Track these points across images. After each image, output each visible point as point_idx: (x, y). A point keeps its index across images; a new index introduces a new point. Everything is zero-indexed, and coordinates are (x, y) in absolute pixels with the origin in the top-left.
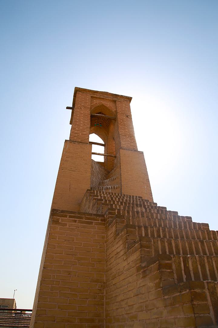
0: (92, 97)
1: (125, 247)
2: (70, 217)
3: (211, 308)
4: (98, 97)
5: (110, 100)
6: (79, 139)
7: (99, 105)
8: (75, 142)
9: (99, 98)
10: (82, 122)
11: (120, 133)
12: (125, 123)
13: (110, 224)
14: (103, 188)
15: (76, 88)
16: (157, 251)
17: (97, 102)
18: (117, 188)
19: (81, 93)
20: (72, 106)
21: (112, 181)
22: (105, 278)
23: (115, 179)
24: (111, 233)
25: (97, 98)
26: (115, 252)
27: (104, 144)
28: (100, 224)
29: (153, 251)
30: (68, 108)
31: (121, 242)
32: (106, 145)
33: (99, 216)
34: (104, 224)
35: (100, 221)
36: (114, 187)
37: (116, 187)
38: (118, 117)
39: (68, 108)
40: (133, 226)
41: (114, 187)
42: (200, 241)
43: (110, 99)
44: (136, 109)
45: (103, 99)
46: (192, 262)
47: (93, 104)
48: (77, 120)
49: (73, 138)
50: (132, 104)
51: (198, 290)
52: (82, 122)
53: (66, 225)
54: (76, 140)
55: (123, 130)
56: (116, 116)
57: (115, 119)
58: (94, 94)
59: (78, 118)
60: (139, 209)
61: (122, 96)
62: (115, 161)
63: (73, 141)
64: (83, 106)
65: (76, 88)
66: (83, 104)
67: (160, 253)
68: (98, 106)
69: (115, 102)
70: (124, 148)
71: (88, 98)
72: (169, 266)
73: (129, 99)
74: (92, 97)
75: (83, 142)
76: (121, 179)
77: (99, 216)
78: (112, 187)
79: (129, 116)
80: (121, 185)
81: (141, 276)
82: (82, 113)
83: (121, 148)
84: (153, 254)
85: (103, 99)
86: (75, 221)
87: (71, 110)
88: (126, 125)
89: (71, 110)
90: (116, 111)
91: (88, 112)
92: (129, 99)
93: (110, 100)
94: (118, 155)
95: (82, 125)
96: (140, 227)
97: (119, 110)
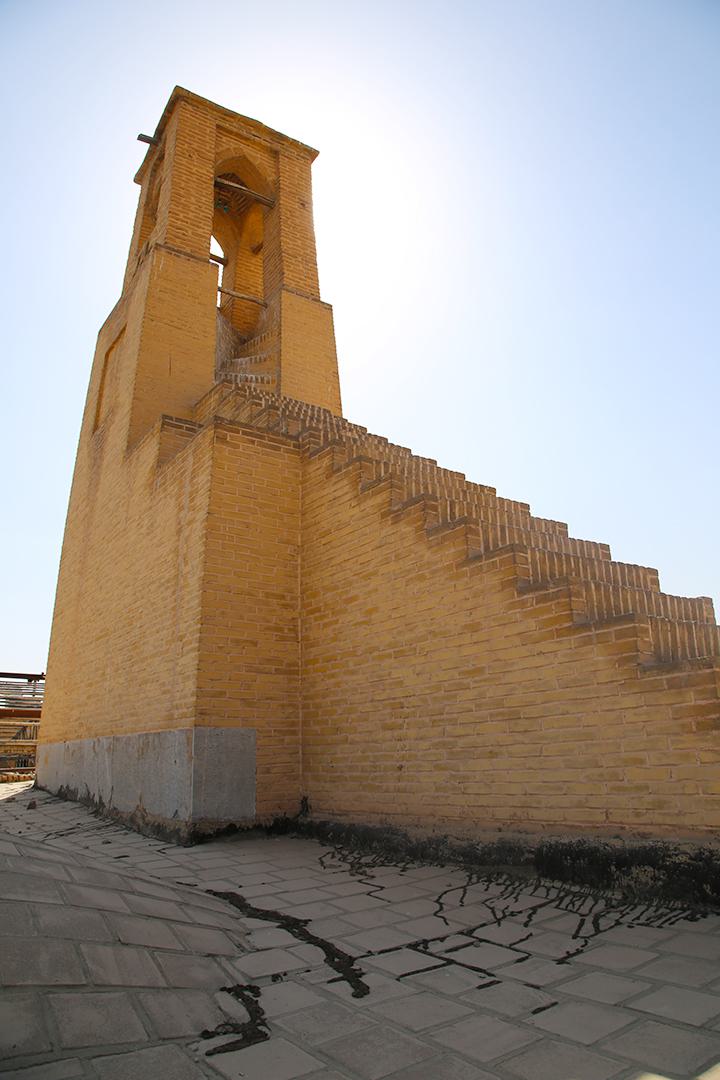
0: (218, 126)
1: (356, 489)
2: (244, 433)
3: (482, 543)
4: (235, 130)
5: (264, 148)
6: (188, 245)
7: (234, 155)
8: (180, 252)
9: (237, 135)
10: (193, 200)
11: (284, 248)
12: (297, 221)
13: (312, 455)
14: (236, 376)
15: (177, 88)
16: (410, 494)
17: (230, 145)
18: (268, 382)
19: (190, 107)
20: (151, 134)
21: (256, 362)
22: (299, 539)
23: (265, 360)
24: (318, 469)
25: (231, 132)
26: (331, 497)
27: (222, 256)
28: (292, 452)
29: (405, 493)
30: (142, 138)
31: (345, 482)
32: (231, 264)
33: (291, 437)
34: (298, 453)
35: (292, 448)
36: (262, 379)
37: (265, 379)
38: (281, 202)
39: (142, 138)
40: (370, 460)
41: (262, 379)
42: (463, 490)
43: (263, 142)
44: (326, 185)
45: (247, 139)
46: (460, 509)
47: (221, 149)
48: (182, 192)
49: (173, 240)
50: (316, 167)
51: (473, 526)
52: (193, 200)
53: (237, 447)
54: (179, 247)
55: (290, 239)
56: (277, 198)
57: (271, 205)
58: (227, 122)
59: (182, 186)
60: (349, 434)
61: (294, 143)
62: (264, 316)
63: (174, 250)
64: (197, 151)
65: (177, 88)
66: (195, 146)
67: (414, 496)
68: (233, 158)
69: (275, 154)
70: (289, 288)
71: (208, 130)
72: (435, 508)
73: (312, 154)
74: (218, 126)
75: (196, 255)
76: (280, 363)
77: (291, 437)
78: (257, 379)
79: (305, 204)
80: (280, 376)
81: (390, 522)
82: (193, 171)
83: (283, 287)
84: (406, 497)
85: (247, 139)
86: (253, 442)
87: (148, 145)
88: (300, 228)
89: (148, 145)
90: (277, 183)
91: (208, 172)
92: (312, 154)
93: (264, 148)
94: (272, 303)
95: (192, 208)
96: (378, 462)
97: (284, 183)
